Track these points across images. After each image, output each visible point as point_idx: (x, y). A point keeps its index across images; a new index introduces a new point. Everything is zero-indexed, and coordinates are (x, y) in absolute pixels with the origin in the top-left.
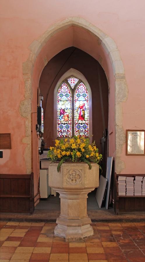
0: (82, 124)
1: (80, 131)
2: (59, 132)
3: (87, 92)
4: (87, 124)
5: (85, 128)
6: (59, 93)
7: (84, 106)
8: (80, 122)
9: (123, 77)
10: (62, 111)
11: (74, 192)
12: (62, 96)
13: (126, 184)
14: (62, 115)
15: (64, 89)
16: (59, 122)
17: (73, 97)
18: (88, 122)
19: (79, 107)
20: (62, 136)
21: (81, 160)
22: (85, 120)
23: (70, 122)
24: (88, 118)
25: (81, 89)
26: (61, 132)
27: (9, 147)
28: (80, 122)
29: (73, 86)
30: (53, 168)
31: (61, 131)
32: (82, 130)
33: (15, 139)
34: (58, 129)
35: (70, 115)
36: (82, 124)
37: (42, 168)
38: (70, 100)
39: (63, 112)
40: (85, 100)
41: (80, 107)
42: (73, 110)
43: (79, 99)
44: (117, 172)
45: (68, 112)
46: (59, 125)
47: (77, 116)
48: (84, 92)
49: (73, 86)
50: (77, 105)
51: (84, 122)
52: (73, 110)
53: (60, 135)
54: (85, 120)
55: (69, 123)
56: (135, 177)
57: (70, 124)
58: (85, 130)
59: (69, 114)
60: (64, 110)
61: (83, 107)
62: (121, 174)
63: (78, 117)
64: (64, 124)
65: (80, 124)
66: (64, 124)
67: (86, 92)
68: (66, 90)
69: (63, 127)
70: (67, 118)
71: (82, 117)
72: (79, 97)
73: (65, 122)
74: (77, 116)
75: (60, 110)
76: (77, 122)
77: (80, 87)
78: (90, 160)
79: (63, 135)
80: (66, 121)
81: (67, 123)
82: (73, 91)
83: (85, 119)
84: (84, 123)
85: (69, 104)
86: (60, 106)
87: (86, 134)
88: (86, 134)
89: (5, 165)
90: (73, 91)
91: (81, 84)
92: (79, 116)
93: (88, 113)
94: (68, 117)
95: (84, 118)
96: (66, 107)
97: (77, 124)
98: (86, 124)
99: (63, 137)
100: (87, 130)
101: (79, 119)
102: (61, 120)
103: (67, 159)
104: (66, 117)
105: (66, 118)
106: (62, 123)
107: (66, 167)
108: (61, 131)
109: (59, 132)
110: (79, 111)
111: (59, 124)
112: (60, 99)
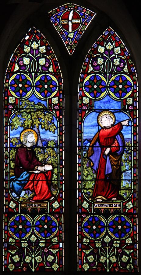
0: (107, 214)
1: (98, 245)
2: (10, 247)
3: (133, 70)
4: (130, 215)
5: (120, 234)
6: (11, 73)
7: (118, 137)
10: (23, 159)
12: (22, 87)
13: (109, 139)
14: (24, 175)
15: (34, 53)
16: (12, 205)
17: (70, 93)
18: (134, 208)
19: (98, 140)
20: (25, 269)
22: (120, 198)
23: (56, 205)
24: (137, 187)
25: (105, 58)
26: (21, 252)
31: (18, 243)
32: (107, 239)
34: (5, 236)
36: (107, 214)
38: (60, 110)
39: (28, 158)
40: (125, 110)
41: (102, 140)
43: (98, 105)
46: (9, 218)
47: (88, 178)
48: (120, 69)
51: (117, 204)
53: (13, 262)
54: (120, 198)
55: (51, 207)
57: (60, 214)
58: (122, 243)
59: (56, 171)
60: (34, 153)
61: (114, 138)
62: (124, 135)
63: (91, 184)
64: (33, 213)
65: (98, 211)
66: (33, 213)
67: (126, 70)
68: (42, 61)
69: (27, 226)
70: (45, 186)
71: (109, 184)
72: (95, 94)
73: (37, 205)
74: (88, 178)
75: (13, 152)
76: (85, 205)
77: (101, 50)
79: (26, 264)
80: (42, 201)
81: (43, 211)
83: (122, 193)
84: (117, 212)
85: (52, 128)
87: (125, 258)
88: (125, 258)
91: (105, 32)
92: (96, 180)
93: (135, 167)
94: (50, 183)
95: (118, 187)
96: (43, 136)
97: (88, 214)
98: (127, 214)
99: (29, 270)
100: (129, 241)
101: (97, 191)
104: (40, 182)
105: (42, 185)
106: (24, 211)
108: (18, 243)
109: (10, 247)
110: (95, 159)
111: (10, 213)
112: (16, 103)
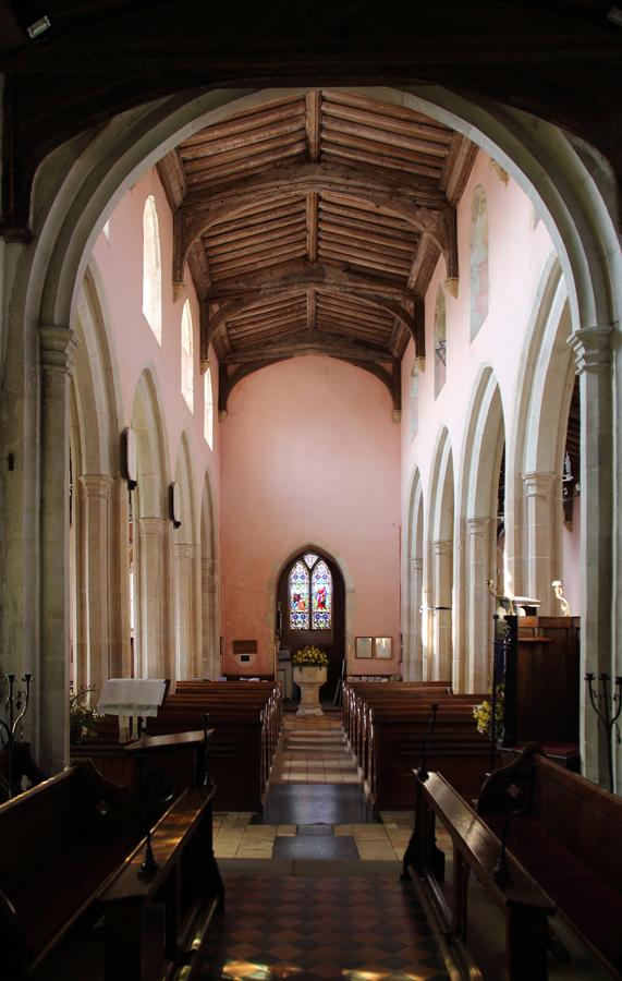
8: (319, 610)
9: (354, 592)
11: (311, 685)
17: (310, 579)
21: (315, 664)
27: (255, 652)
28: (319, 610)
29: (310, 565)
30: (296, 670)
33: (260, 645)
35: (307, 602)
37: (378, 656)
39: (298, 598)
42: (311, 595)
44: (348, 673)
45: (305, 599)
47: (315, 602)
49: (310, 565)
50: (316, 589)
52: (311, 595)
56: (463, 697)
71: (322, 605)
74: (315, 602)
78: (321, 665)
82: (310, 571)
86: (294, 590)
89: (252, 667)
90: (310, 571)
101: (319, 606)
102: (295, 608)
103: (306, 664)
107: (305, 669)
